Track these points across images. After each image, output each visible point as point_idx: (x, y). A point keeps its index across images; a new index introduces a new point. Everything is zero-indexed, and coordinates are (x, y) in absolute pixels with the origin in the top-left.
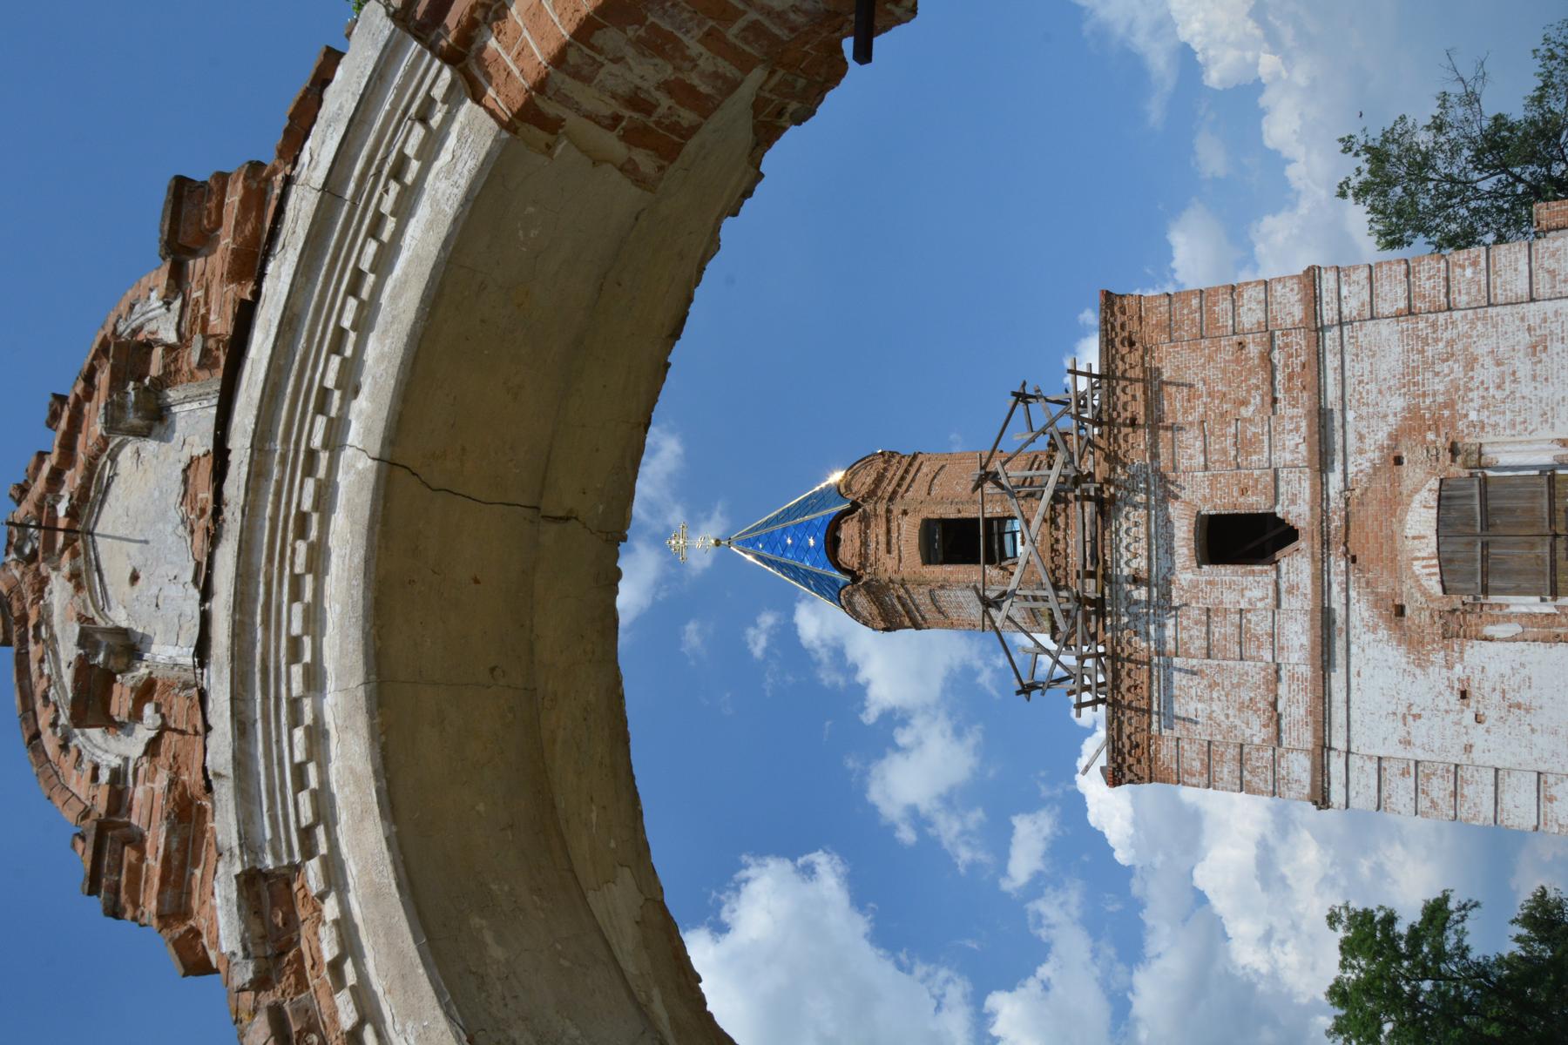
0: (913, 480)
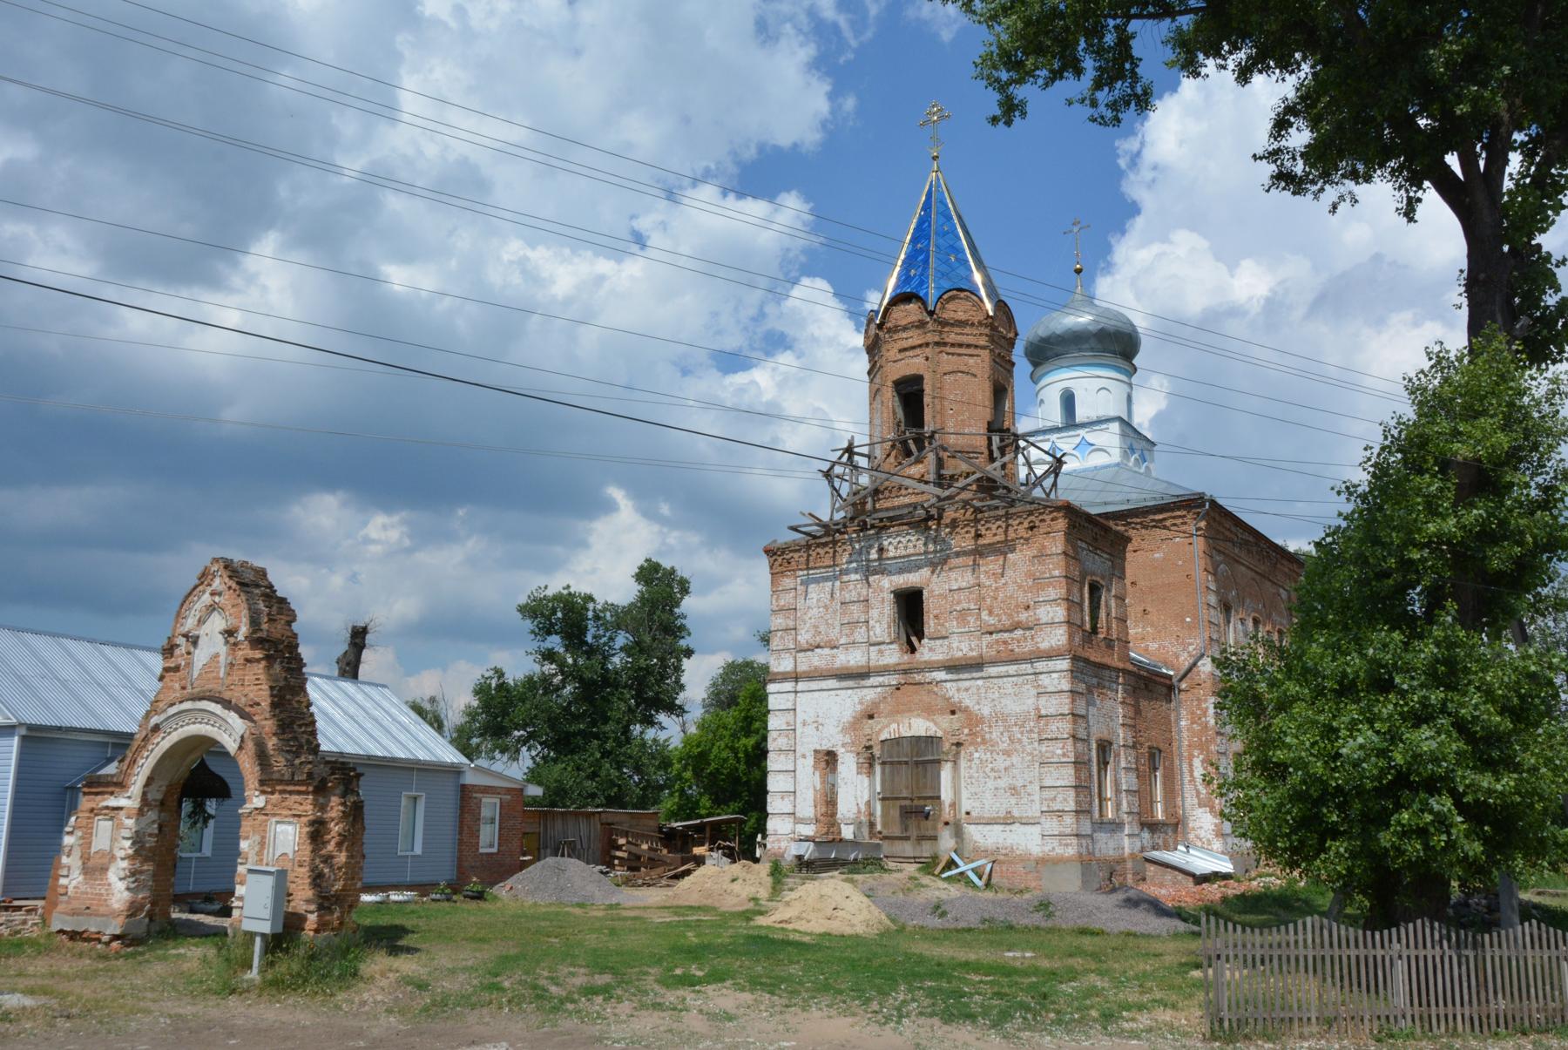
0: (959, 355)
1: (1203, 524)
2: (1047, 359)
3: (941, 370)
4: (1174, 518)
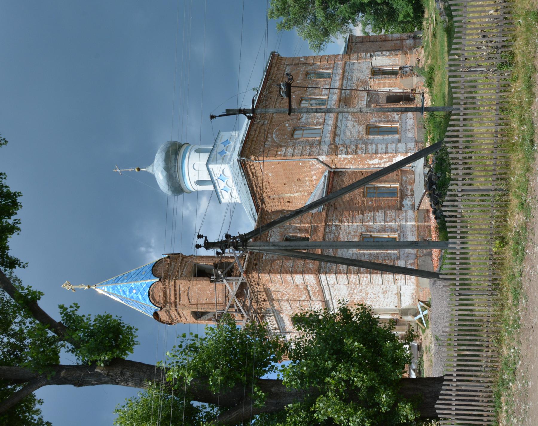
0: (180, 295)
1: (253, 158)
2: (180, 186)
3: (188, 304)
4: (251, 169)
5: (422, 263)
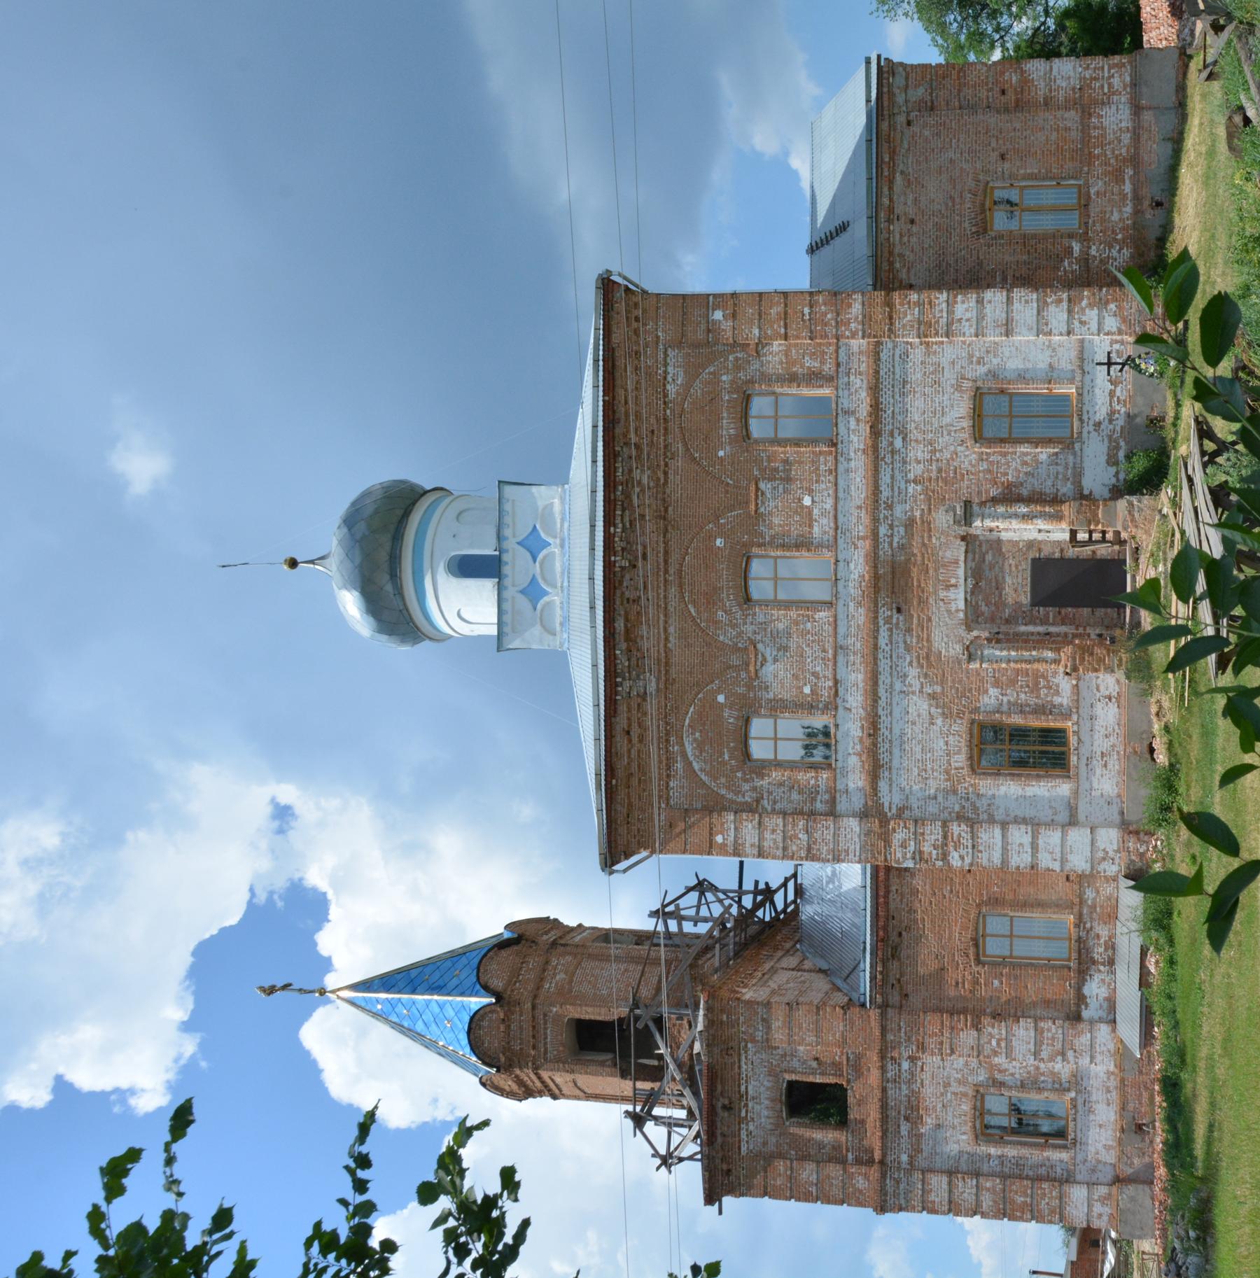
5: (1129, 1205)
